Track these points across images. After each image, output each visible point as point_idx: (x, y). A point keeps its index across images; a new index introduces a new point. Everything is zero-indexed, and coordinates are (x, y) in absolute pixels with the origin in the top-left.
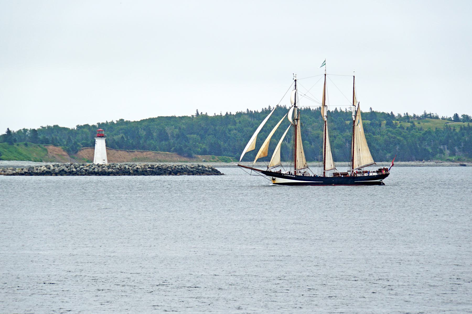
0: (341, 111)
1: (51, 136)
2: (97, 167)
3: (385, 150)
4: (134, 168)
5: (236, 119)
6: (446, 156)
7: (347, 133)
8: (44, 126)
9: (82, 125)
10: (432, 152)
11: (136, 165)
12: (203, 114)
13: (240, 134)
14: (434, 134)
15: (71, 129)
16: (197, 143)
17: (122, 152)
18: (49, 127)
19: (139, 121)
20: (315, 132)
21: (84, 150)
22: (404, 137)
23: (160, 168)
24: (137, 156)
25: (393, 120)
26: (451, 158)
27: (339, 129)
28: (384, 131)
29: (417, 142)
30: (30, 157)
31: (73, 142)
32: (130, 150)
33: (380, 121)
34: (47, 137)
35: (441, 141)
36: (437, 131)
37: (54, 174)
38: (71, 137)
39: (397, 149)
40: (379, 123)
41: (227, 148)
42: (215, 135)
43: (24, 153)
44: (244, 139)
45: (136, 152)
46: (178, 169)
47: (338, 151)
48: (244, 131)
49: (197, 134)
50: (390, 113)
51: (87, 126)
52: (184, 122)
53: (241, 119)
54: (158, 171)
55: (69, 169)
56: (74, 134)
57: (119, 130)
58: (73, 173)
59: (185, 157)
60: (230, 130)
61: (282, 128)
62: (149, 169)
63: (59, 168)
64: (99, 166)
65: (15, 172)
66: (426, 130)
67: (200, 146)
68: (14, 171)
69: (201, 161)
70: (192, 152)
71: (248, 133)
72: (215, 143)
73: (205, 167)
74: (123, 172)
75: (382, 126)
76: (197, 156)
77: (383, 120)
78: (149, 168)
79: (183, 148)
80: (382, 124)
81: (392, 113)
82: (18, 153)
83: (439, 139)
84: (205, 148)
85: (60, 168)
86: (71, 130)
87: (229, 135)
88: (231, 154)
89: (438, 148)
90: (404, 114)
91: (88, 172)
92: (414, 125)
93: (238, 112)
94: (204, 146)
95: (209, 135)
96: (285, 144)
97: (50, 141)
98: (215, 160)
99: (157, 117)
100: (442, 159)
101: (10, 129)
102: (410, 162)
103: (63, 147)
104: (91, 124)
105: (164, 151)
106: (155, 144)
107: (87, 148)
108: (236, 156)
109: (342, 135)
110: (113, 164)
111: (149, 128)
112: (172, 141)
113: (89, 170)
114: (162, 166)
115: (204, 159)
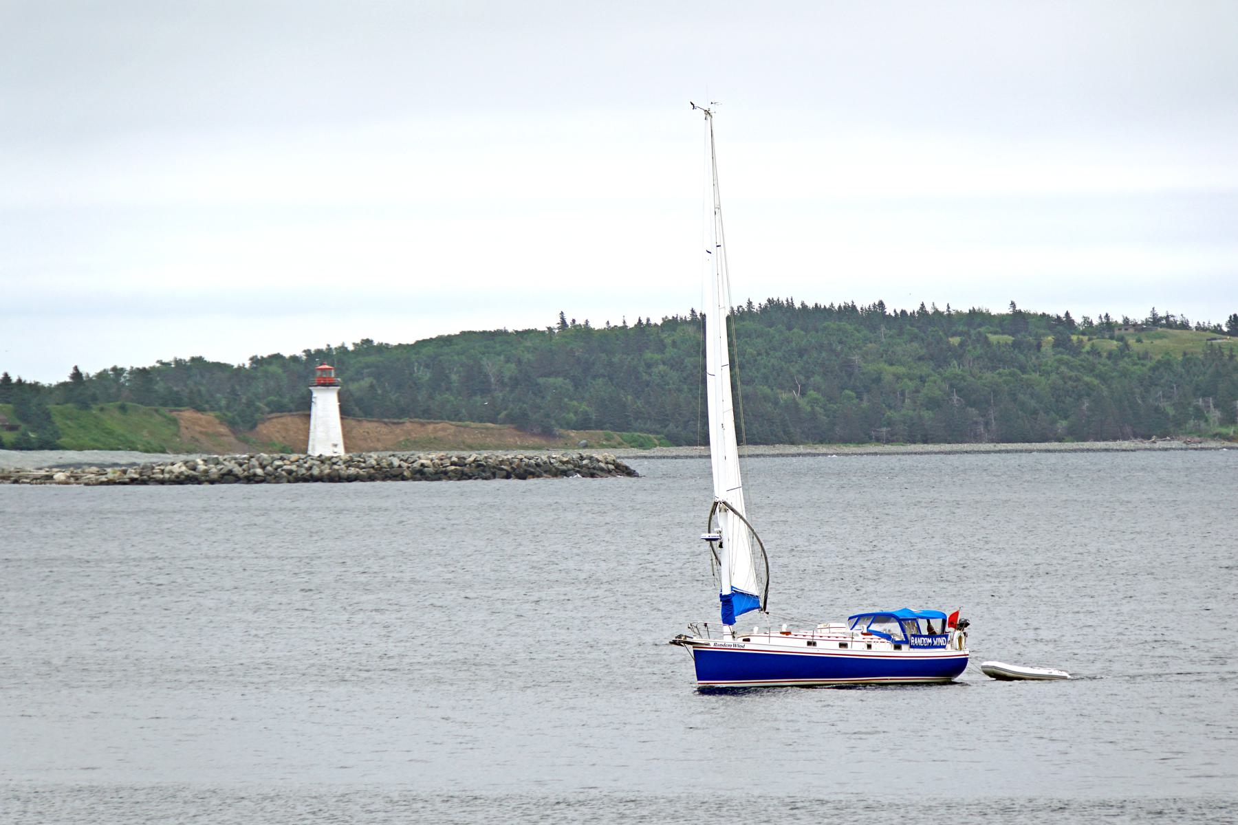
0: (937, 312)
1: (186, 385)
3: (1054, 411)
4: (415, 465)
5: (664, 336)
6: (1212, 426)
7: (955, 367)
8: (166, 360)
9: (265, 356)
10: (1174, 416)
12: (577, 323)
13: (674, 375)
14: (1180, 370)
15: (236, 366)
16: (566, 400)
18: (178, 362)
19: (412, 345)
20: (870, 368)
22: (1103, 378)
23: (482, 465)
24: (410, 435)
25: (1073, 334)
26: (1224, 430)
27: (932, 357)
28: (1050, 363)
29: (1137, 390)
30: (135, 440)
32: (394, 418)
33: (1038, 337)
34: (175, 389)
35: (1197, 388)
36: (1188, 360)
39: (1084, 407)
40: (1035, 343)
42: (611, 379)
43: (119, 430)
46: (528, 465)
47: (932, 415)
50: (1062, 315)
51: (278, 357)
52: (528, 344)
53: (677, 335)
55: (244, 470)
58: (256, 479)
59: (533, 435)
60: (649, 366)
61: (785, 357)
62: (453, 467)
63: (220, 467)
64: (322, 460)
65: (106, 480)
66: (1159, 357)
67: (574, 406)
68: (104, 476)
69: (576, 446)
70: (553, 422)
73: (598, 461)
75: (1043, 349)
77: (1045, 335)
78: (453, 464)
79: (530, 414)
80: (1043, 344)
81: (1067, 314)
83: (1191, 382)
85: (222, 466)
86: (236, 369)
87: (645, 377)
89: (1189, 404)
90: (1100, 317)
92: (1127, 346)
93: (666, 317)
94: (584, 407)
95: (594, 377)
96: (794, 399)
97: (186, 399)
98: (613, 443)
100: (1202, 434)
101: (81, 370)
102: (1118, 442)
103: (218, 413)
104: (287, 354)
105: (481, 422)
106: (455, 403)
107: (281, 417)
108: (666, 431)
109: (940, 374)
110: (360, 456)
113: (296, 472)
114: (486, 458)
115: (584, 441)
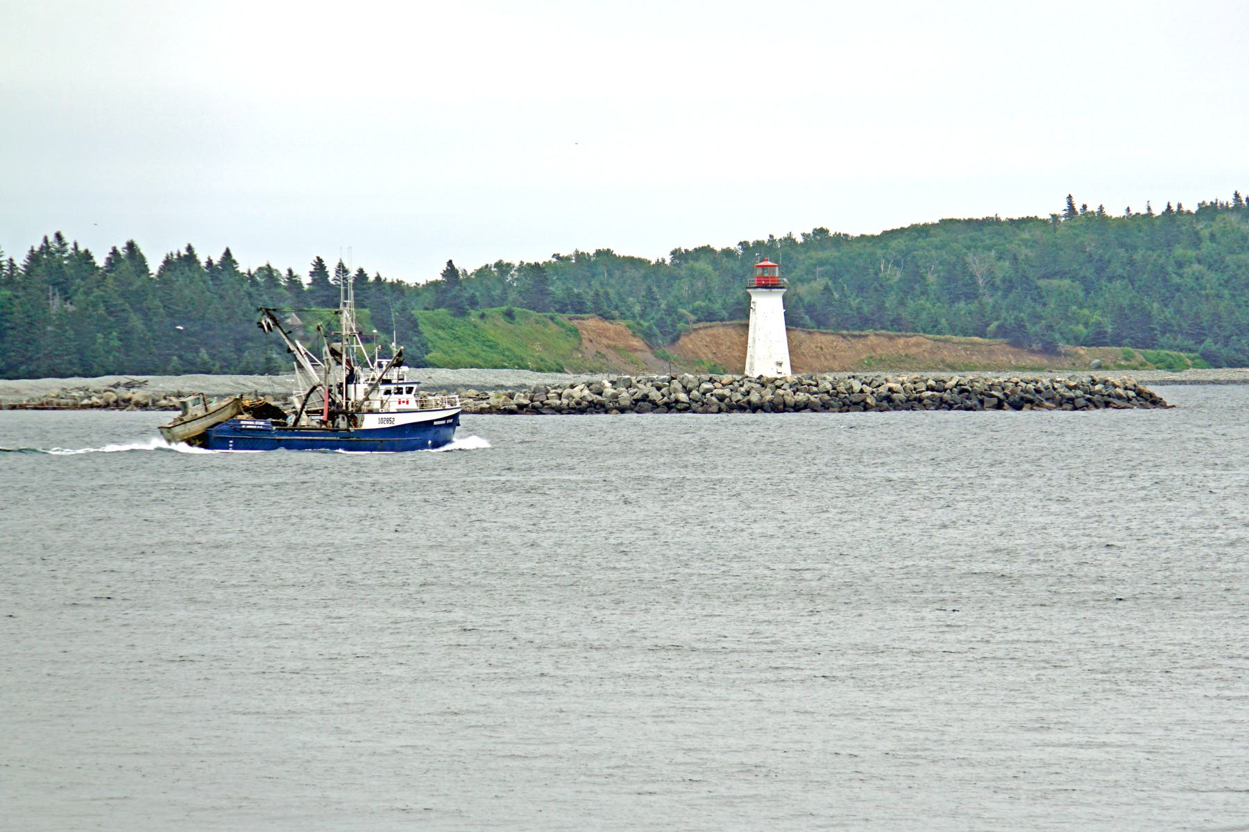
2: (758, 386)
4: (881, 389)
5: (1199, 227)
9: (691, 249)
11: (887, 380)
12: (1089, 209)
13: (1212, 277)
15: (653, 262)
17: (824, 338)
18: (580, 256)
21: (701, 332)
23: (966, 390)
24: (875, 352)
30: (524, 355)
31: (663, 306)
37: (615, 411)
38: (655, 289)
41: (1173, 322)
43: (504, 343)
44: (1226, 292)
45: (872, 338)
48: (1227, 266)
49: (1074, 279)
51: (706, 250)
52: (1026, 236)
54: (958, 398)
55: (663, 395)
56: (666, 279)
57: (815, 266)
58: (679, 406)
59: (1033, 352)
60: (1180, 265)
62: (929, 393)
63: (632, 391)
64: (762, 382)
70: (1057, 336)
71: (1239, 272)
72: (1132, 307)
73: (1115, 386)
74: (844, 404)
76: (1074, 350)
78: (929, 388)
82: (484, 343)
84: (1099, 324)
85: (636, 390)
87: (1176, 280)
88: (1186, 343)
91: (727, 405)
93: (1204, 203)
94: (1096, 317)
95: (1110, 279)
98: (1133, 363)
99: (937, 221)
103: (631, 322)
106: (933, 311)
108: (1201, 348)
110: (811, 378)
111: (914, 257)
112: (991, 301)
114: (972, 381)
115: (1097, 361)
